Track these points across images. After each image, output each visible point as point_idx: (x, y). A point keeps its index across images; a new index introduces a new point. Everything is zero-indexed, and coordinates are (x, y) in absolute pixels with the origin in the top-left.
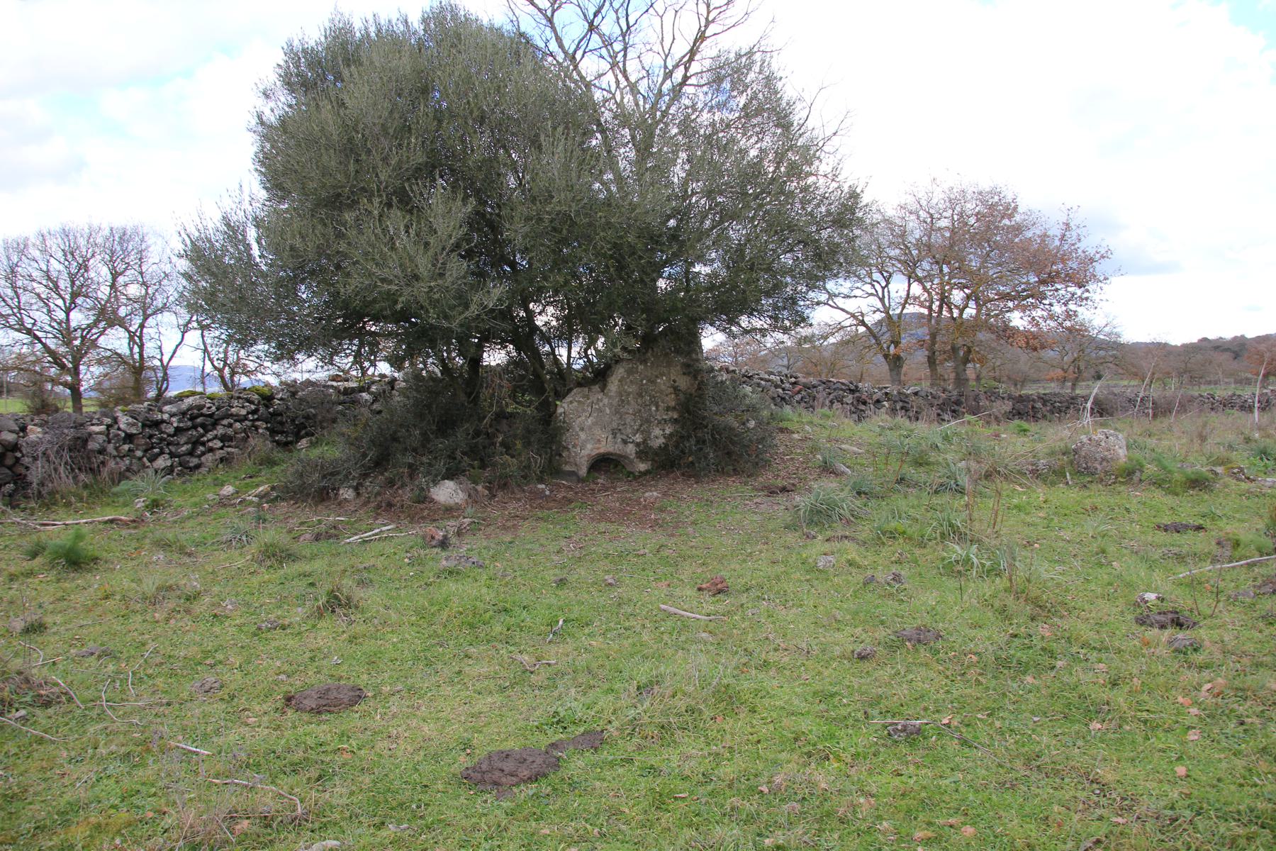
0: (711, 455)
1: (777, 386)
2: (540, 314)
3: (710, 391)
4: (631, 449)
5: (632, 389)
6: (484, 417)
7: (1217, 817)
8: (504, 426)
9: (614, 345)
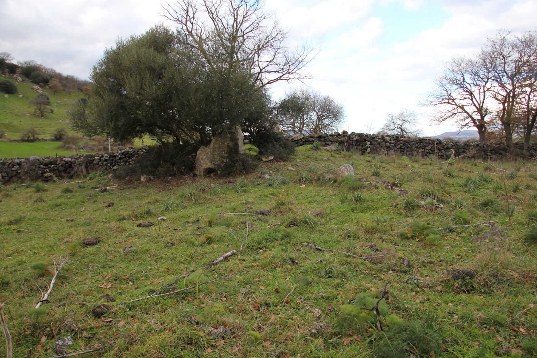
5: (217, 146)
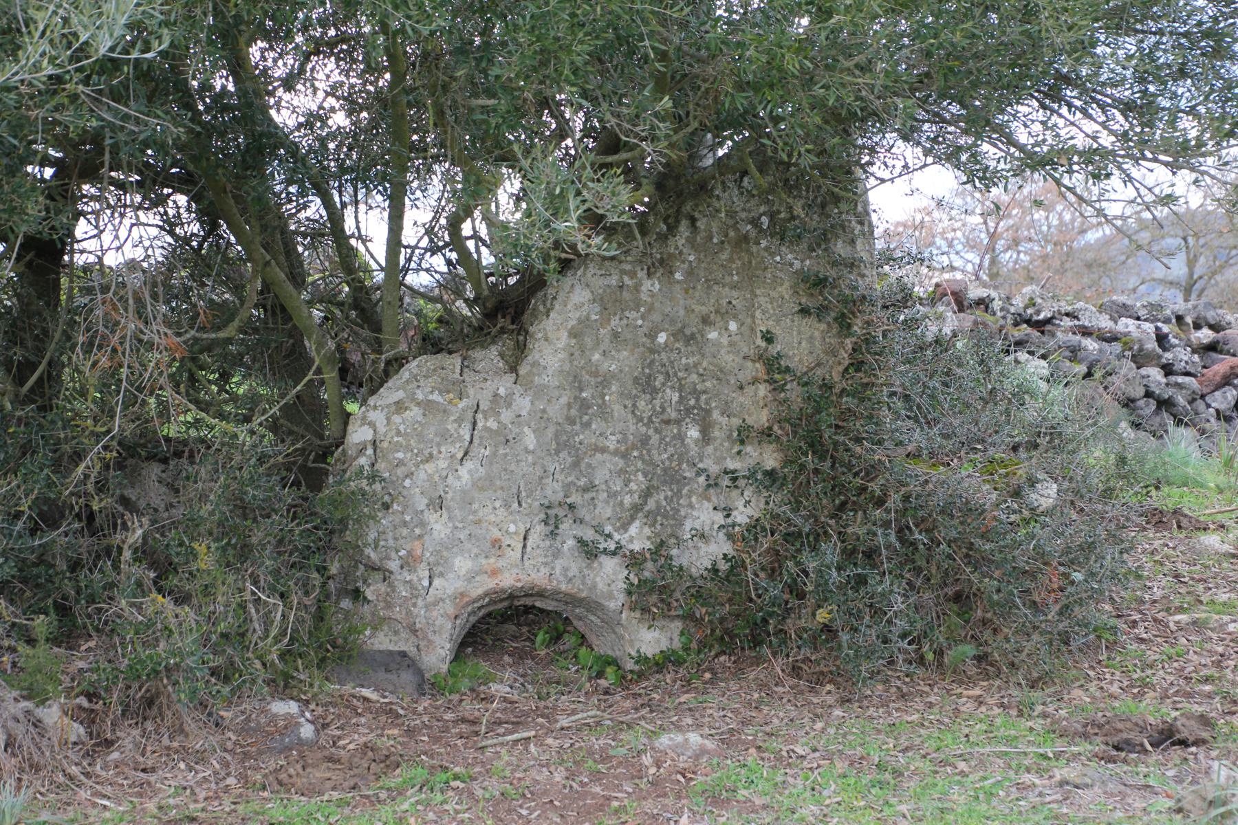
0: (899, 604)
1: (1140, 359)
2: (289, 83)
3: (895, 375)
4: (609, 578)
5: (623, 361)
6: (78, 457)
7: (604, 711)
8: (152, 485)
9: (556, 205)
